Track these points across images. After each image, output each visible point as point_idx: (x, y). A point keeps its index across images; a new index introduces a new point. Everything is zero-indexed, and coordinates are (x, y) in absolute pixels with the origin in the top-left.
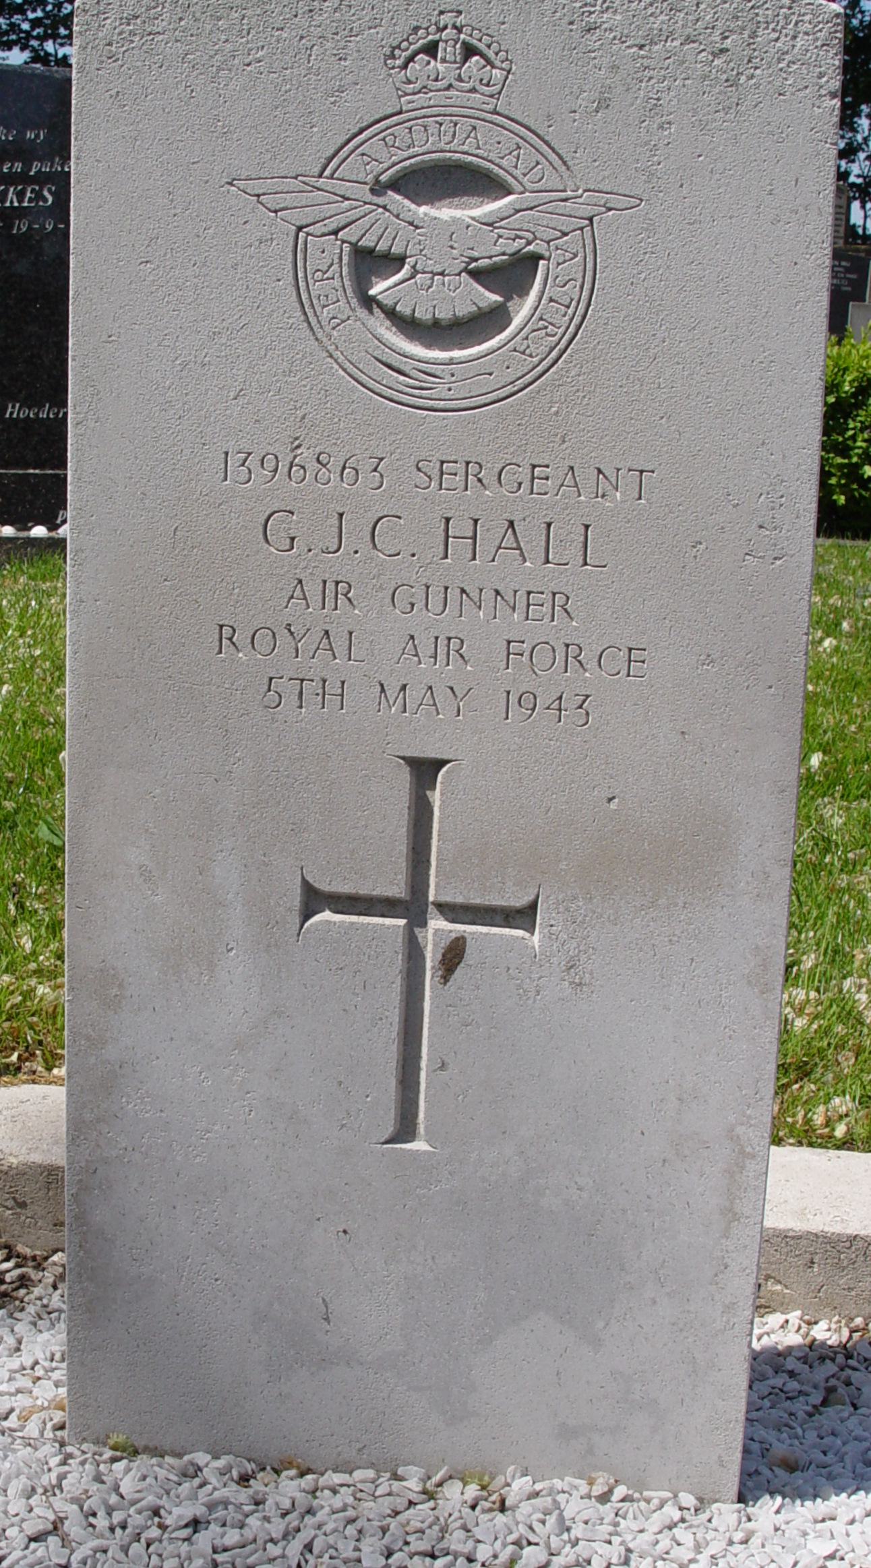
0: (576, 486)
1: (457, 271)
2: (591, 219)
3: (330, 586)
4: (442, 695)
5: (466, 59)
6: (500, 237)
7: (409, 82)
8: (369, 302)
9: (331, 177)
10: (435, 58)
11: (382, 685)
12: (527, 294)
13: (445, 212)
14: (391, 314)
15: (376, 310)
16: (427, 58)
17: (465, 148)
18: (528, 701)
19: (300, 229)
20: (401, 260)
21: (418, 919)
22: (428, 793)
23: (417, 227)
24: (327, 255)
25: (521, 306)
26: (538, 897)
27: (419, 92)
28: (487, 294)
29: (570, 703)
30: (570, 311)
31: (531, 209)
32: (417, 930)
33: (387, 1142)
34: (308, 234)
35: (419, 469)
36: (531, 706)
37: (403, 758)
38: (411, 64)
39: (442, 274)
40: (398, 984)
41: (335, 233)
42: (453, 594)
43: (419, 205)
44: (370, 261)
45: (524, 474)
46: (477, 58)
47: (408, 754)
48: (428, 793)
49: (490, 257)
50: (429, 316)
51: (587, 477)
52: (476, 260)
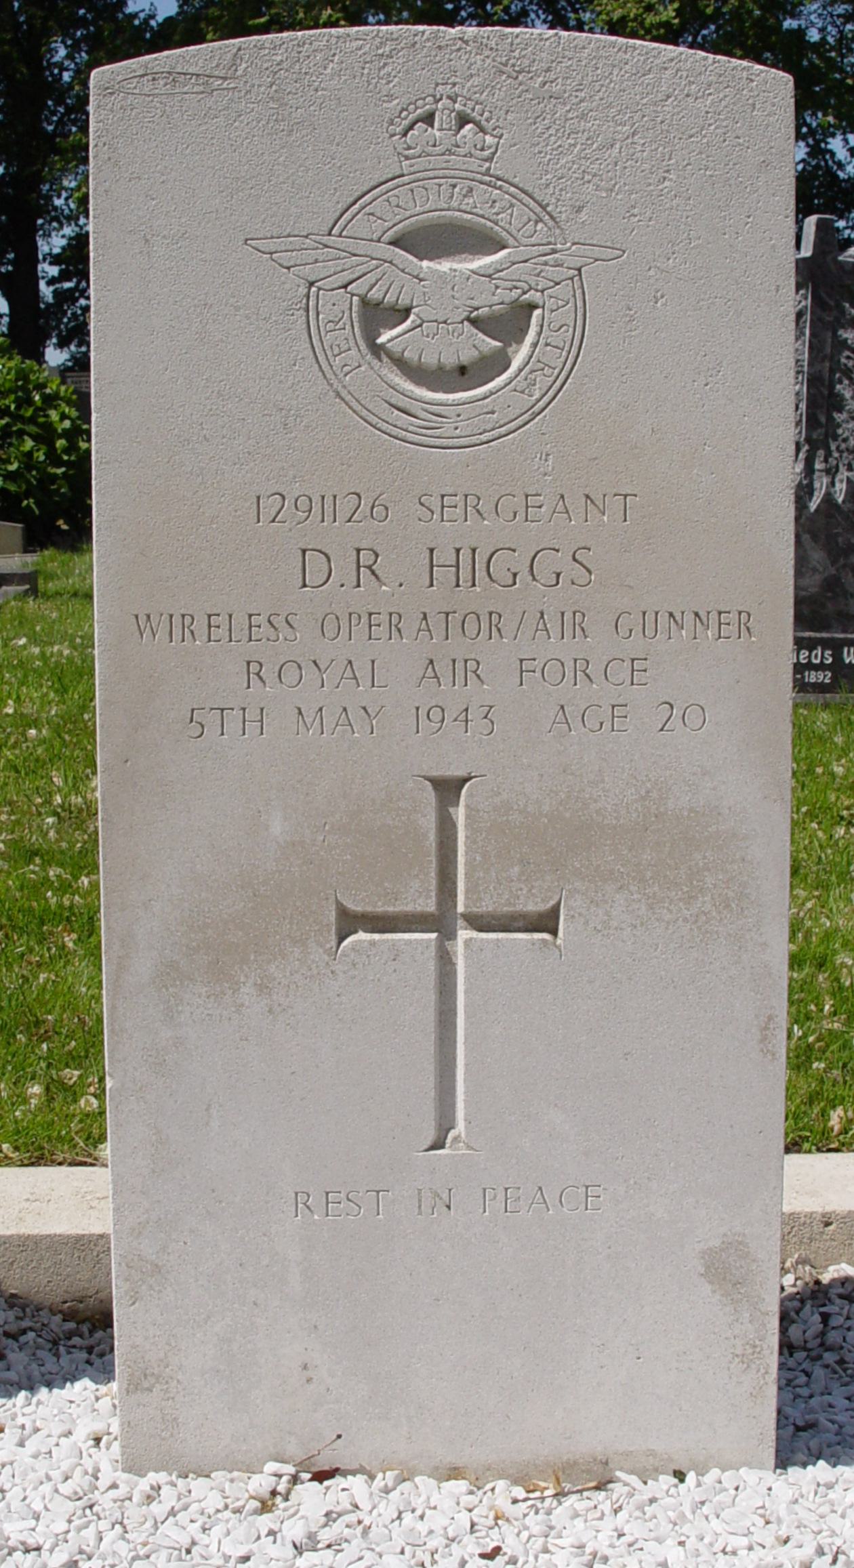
0: (567, 512)
2: (579, 270)
3: (177, 620)
4: (355, 714)
5: (461, 127)
6: (497, 287)
7: (409, 148)
8: (377, 350)
9: (340, 236)
10: (432, 126)
13: (445, 266)
14: (401, 364)
15: (383, 356)
16: (425, 126)
18: (436, 714)
19: (312, 284)
20: (407, 311)
21: (448, 934)
22: (451, 810)
23: (421, 280)
24: (338, 307)
25: (516, 352)
26: (559, 904)
28: (488, 340)
31: (526, 261)
33: (427, 1150)
34: (319, 289)
35: (422, 504)
36: (440, 718)
38: (411, 132)
39: (445, 322)
40: (431, 998)
41: (345, 287)
42: (663, 619)
43: (421, 260)
44: (377, 315)
46: (469, 127)
47: (434, 774)
49: (490, 306)
51: (576, 503)
52: (477, 309)
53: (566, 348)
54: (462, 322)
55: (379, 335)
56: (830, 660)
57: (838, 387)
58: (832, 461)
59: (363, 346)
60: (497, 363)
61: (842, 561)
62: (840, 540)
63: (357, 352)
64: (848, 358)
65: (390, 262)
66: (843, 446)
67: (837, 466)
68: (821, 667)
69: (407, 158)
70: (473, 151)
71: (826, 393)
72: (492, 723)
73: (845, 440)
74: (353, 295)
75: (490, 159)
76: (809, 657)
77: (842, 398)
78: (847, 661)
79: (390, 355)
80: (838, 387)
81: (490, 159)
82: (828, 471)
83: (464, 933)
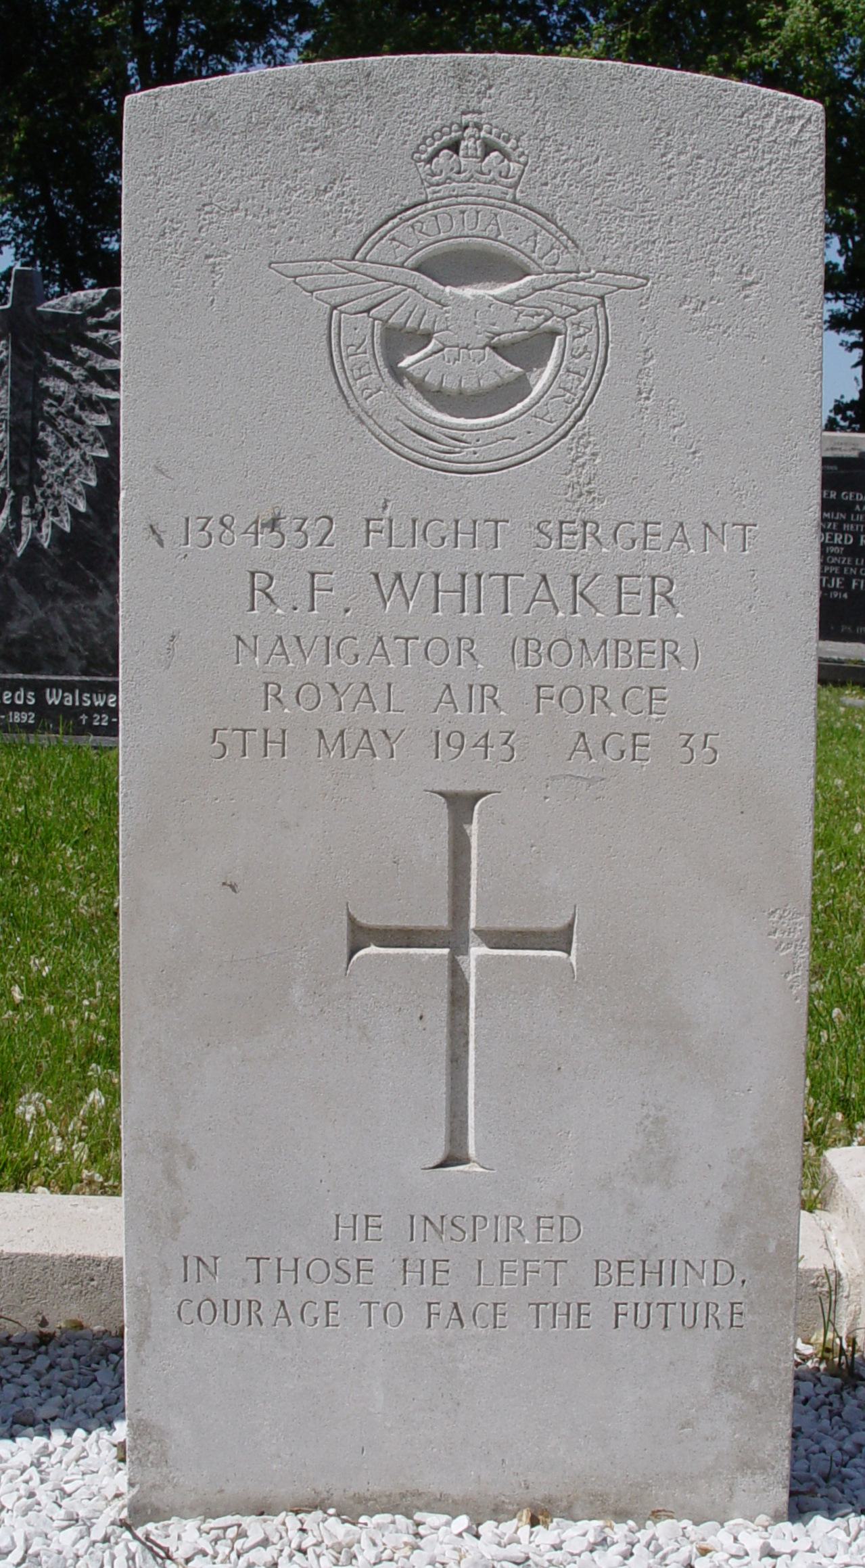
1: (481, 345)
2: (602, 298)
4: (377, 738)
5: (486, 154)
7: (433, 175)
8: (398, 375)
9: (364, 260)
10: (457, 153)
11: (321, 732)
12: (546, 365)
13: (468, 292)
14: (420, 386)
17: (486, 234)
19: (335, 308)
20: (428, 337)
22: (466, 826)
24: (360, 332)
27: (444, 183)
28: (513, 367)
29: (496, 739)
30: (585, 381)
31: (550, 288)
32: (460, 958)
34: (341, 312)
37: (441, 794)
41: (368, 311)
43: (445, 285)
44: (398, 340)
45: (637, 529)
47: (443, 788)
48: (466, 826)
50: (455, 387)
51: (694, 530)
52: (499, 335)
53: (588, 376)
54: (484, 348)
55: (402, 359)
56: (33, 702)
57: (41, 434)
58: (38, 507)
59: (385, 371)
60: (515, 390)
61: (50, 605)
62: (47, 584)
63: (378, 375)
64: (51, 405)
65: (414, 288)
66: (49, 492)
67: (43, 512)
68: (25, 708)
69: (432, 185)
70: (498, 179)
71: (29, 440)
72: (692, 751)
73: (50, 486)
74: (375, 319)
75: (515, 186)
76: (12, 698)
77: (47, 446)
78: (50, 702)
79: (412, 379)
80: (41, 434)
81: (515, 186)
82: (33, 517)
83: (477, 951)
